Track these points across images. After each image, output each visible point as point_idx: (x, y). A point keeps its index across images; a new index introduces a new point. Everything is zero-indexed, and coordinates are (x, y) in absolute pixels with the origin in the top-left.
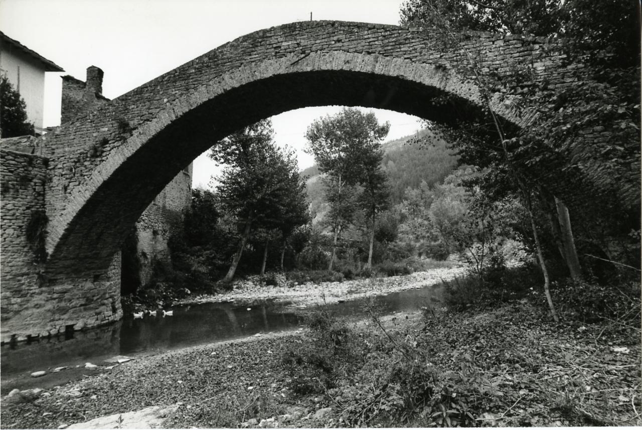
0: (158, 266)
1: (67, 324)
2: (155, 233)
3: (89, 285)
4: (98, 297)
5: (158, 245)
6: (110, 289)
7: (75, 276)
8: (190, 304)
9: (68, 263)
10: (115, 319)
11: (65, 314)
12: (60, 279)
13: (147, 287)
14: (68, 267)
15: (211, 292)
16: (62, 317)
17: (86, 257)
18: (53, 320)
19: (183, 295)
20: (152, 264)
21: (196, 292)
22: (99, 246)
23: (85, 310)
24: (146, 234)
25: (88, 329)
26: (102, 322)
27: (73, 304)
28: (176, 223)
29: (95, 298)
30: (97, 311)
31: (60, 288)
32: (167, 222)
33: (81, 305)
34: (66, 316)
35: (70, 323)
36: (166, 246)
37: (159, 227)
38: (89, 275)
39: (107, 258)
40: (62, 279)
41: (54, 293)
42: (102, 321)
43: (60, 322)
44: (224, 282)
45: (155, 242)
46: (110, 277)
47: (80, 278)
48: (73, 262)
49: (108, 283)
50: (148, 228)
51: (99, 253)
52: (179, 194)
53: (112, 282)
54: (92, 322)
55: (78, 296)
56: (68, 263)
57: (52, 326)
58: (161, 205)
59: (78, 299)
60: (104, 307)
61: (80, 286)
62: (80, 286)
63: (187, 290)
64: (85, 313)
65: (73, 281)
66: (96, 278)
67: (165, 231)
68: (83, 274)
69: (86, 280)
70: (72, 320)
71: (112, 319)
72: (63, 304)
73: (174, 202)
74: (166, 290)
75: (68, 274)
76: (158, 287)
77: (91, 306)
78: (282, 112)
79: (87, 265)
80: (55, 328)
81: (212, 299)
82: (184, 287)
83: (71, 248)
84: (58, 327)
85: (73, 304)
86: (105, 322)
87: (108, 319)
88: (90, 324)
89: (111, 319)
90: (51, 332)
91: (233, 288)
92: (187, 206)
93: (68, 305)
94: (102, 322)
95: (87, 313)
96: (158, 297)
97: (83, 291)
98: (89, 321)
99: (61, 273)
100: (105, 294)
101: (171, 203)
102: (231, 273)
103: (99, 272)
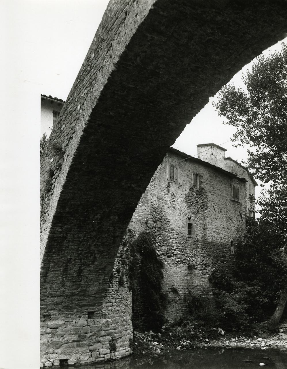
0: (194, 304)
1: (60, 358)
2: (191, 268)
3: (82, 321)
4: (91, 334)
5: (194, 280)
6: (106, 327)
7: (68, 313)
8: (225, 347)
9: (56, 300)
10: (114, 358)
11: (58, 348)
12: (54, 315)
13: (173, 325)
14: (57, 304)
15: (250, 334)
16: (56, 351)
17: (73, 294)
18: (47, 353)
19: (217, 336)
20: (185, 300)
21: (231, 333)
22: (82, 283)
23: (78, 346)
24: (179, 269)
25: (81, 365)
26: (97, 360)
27: (66, 339)
28: (224, 256)
29: (88, 335)
30: (91, 348)
31: (52, 323)
32: (209, 256)
33: (74, 341)
34: (59, 351)
35: (65, 357)
36: (206, 281)
37: (198, 261)
38: (82, 312)
39: (97, 296)
40: (55, 315)
41: (47, 328)
42: (96, 358)
43: (54, 355)
44: (269, 324)
45: (191, 278)
46: (105, 315)
47: (73, 314)
48: (61, 299)
49: (104, 321)
50: (182, 262)
51: (85, 290)
52: (225, 224)
53: (109, 320)
54: (85, 358)
55: (69, 333)
56: (56, 300)
57: (46, 358)
58: (199, 237)
59: (70, 334)
60: (99, 344)
61: (74, 322)
62: (74, 322)
63: (220, 330)
64: (78, 349)
65: (66, 316)
66: (91, 315)
67: (206, 265)
68: (75, 310)
69: (80, 317)
70: (66, 355)
71: (109, 357)
72: (56, 339)
73: (218, 234)
74: (195, 329)
75: (59, 310)
76: (185, 325)
77: (85, 342)
78: (244, 66)
79: (77, 302)
80: (49, 361)
81: (249, 343)
82: (217, 327)
83: (54, 286)
84: (52, 360)
85: (66, 339)
86: (100, 359)
87: (104, 357)
88: (83, 360)
89: (107, 357)
90: (46, 364)
91: (279, 332)
92: (239, 237)
93: (61, 340)
94: (97, 360)
95: (80, 349)
96: (184, 337)
97: (76, 328)
98: (82, 357)
99: (52, 309)
100: (99, 331)
101: (214, 234)
102: (278, 313)
103: (92, 309)
